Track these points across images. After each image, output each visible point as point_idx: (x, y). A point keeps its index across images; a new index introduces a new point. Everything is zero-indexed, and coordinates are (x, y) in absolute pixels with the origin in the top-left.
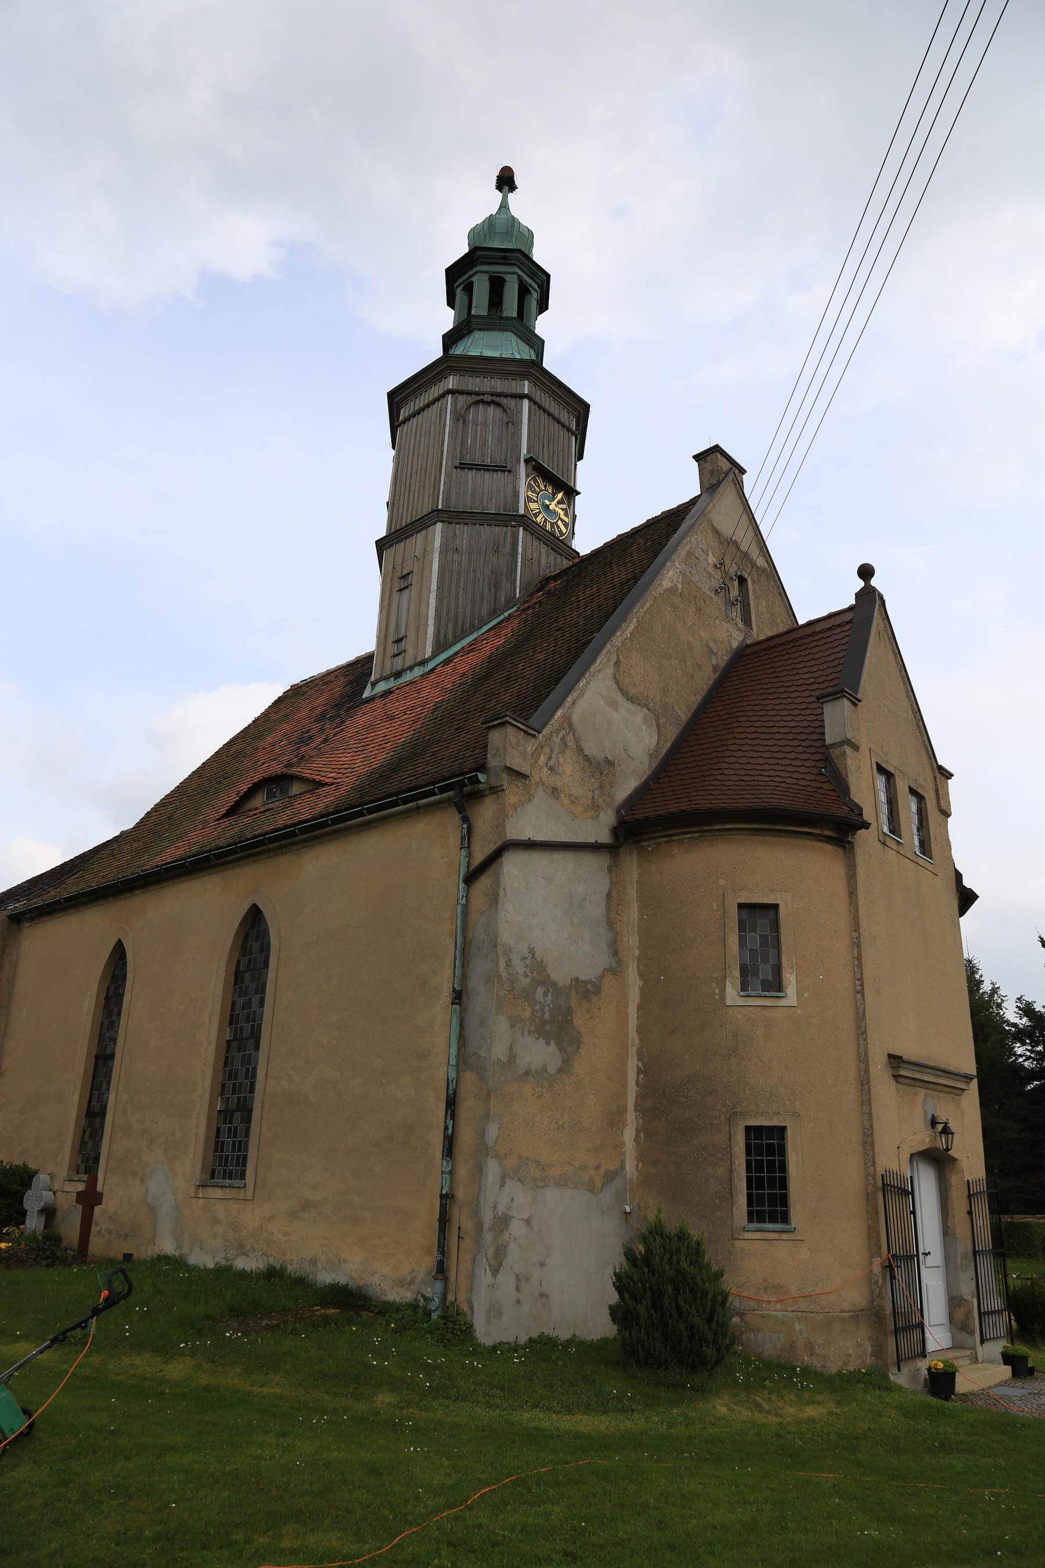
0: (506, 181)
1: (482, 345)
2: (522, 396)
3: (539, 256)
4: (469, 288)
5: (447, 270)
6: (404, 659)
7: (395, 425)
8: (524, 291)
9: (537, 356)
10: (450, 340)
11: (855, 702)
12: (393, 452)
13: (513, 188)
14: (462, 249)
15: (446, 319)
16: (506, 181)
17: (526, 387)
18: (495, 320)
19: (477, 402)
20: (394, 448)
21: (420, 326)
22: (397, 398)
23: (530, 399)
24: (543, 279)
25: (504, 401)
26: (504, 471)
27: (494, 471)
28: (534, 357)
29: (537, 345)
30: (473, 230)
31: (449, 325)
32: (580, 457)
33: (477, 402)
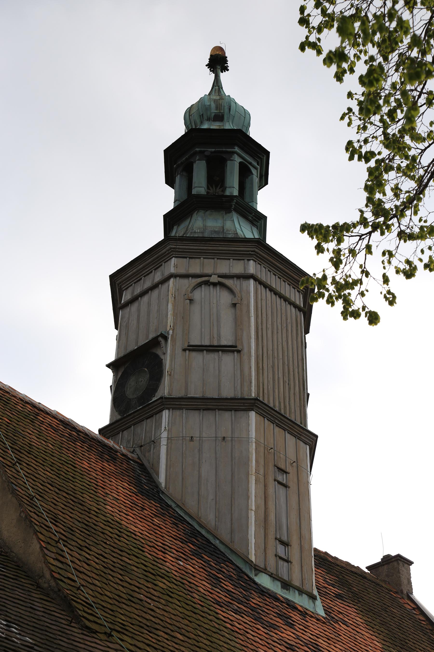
0: (218, 62)
1: (202, 224)
2: (248, 277)
3: (255, 133)
4: (189, 170)
5: (166, 152)
6: (133, 293)
7: (118, 307)
8: (244, 171)
9: (260, 233)
10: (171, 220)
11: (396, 303)
12: (116, 332)
13: (225, 69)
14: (179, 130)
15: (166, 199)
16: (218, 62)
17: (252, 267)
18: (218, 202)
19: (199, 285)
20: (116, 328)
21: (142, 214)
22: (120, 281)
23: (256, 279)
24: (261, 155)
25: (229, 282)
26: (233, 351)
27: (223, 351)
28: (257, 236)
29: (259, 221)
30: (190, 110)
31: (170, 206)
32: (307, 331)
33: (199, 285)
